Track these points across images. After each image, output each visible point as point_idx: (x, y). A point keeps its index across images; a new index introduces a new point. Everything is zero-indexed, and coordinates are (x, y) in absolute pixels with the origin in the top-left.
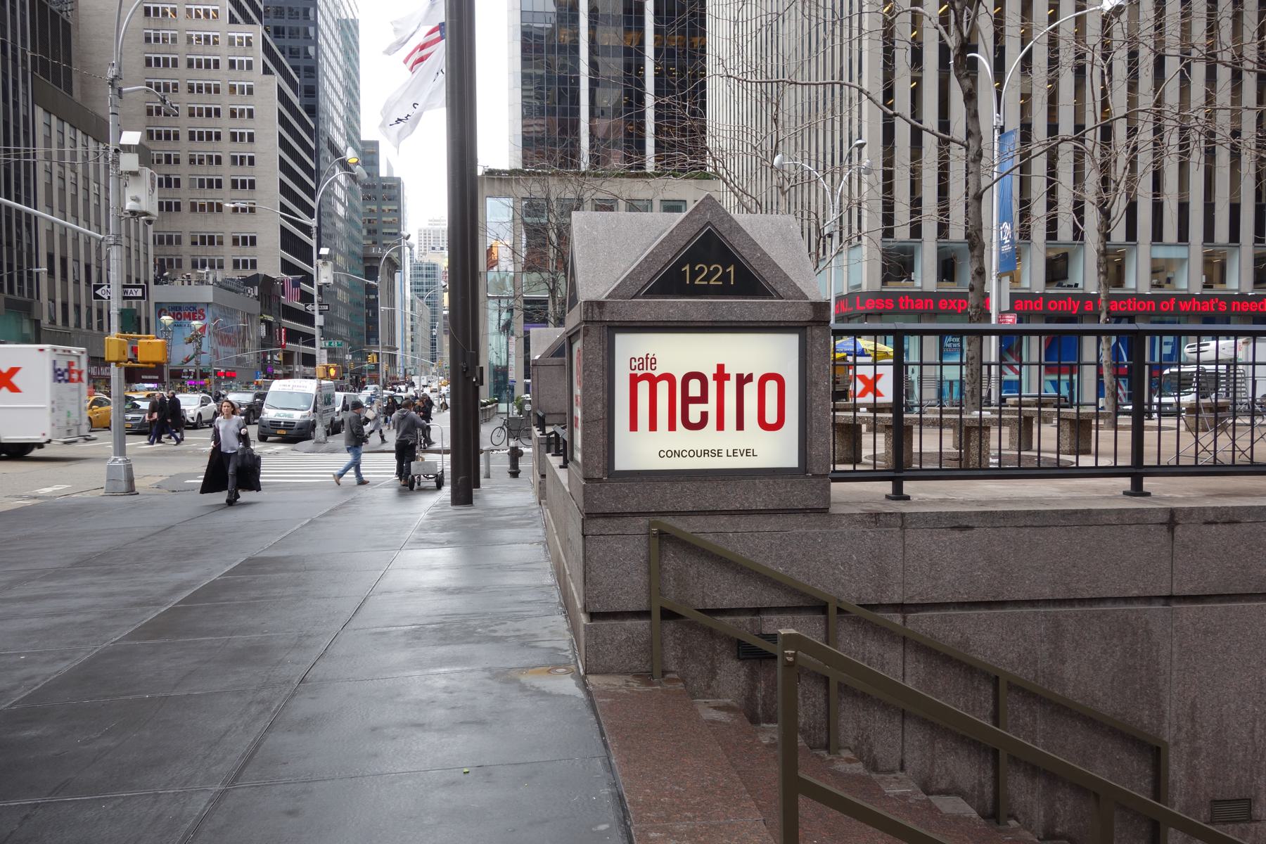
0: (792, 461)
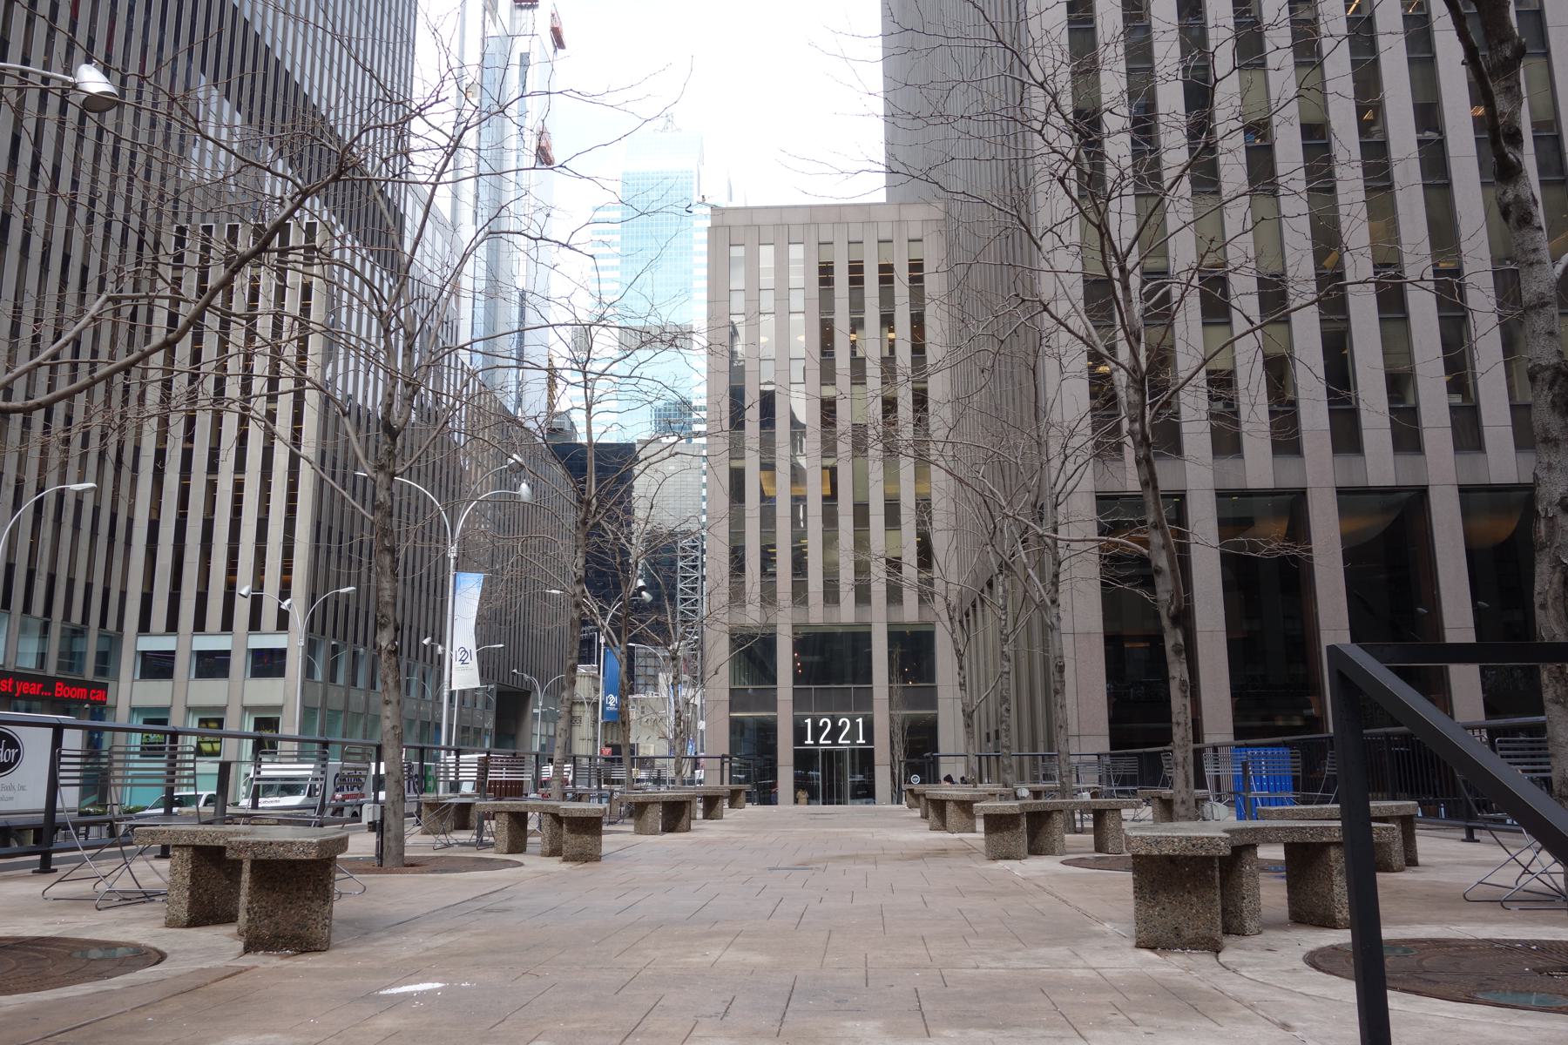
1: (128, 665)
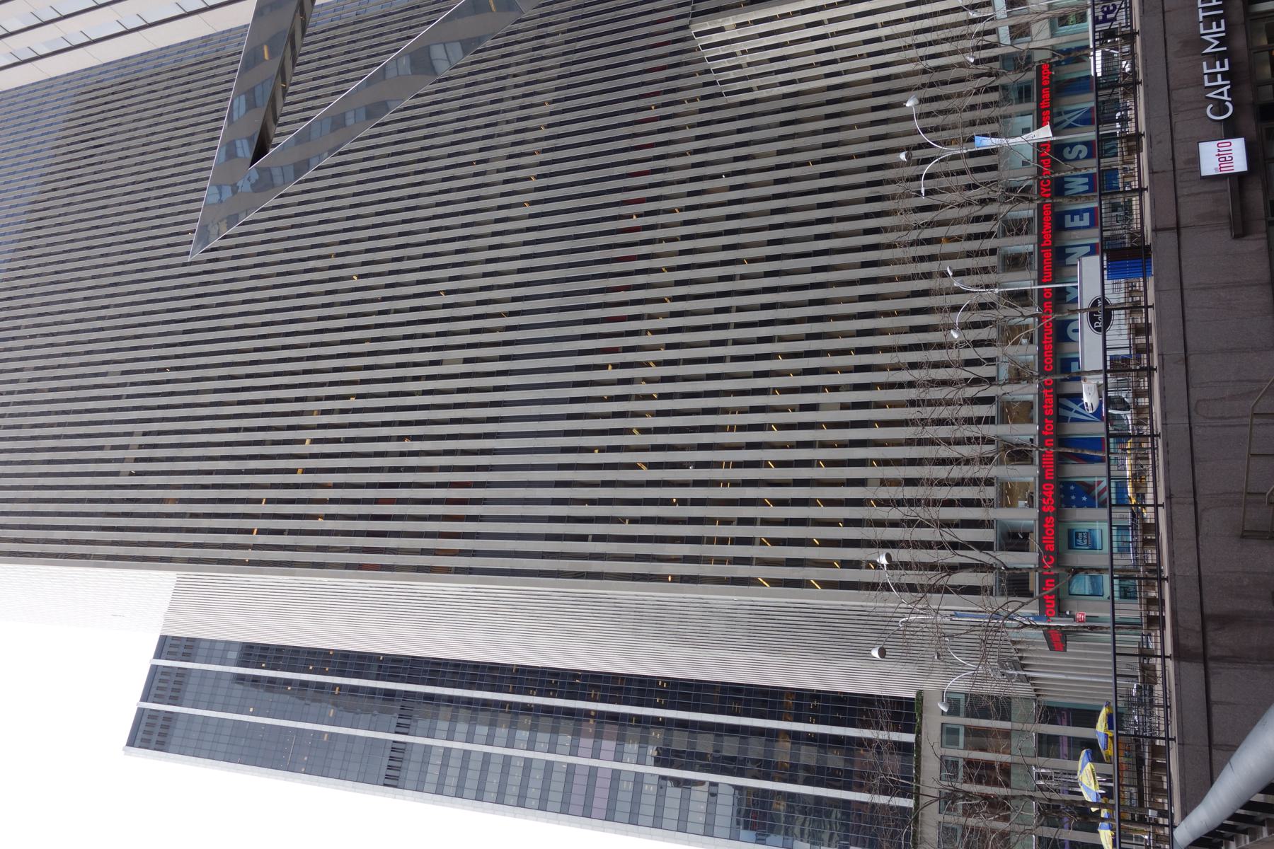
0: (1201, 145)
1: (1022, 45)
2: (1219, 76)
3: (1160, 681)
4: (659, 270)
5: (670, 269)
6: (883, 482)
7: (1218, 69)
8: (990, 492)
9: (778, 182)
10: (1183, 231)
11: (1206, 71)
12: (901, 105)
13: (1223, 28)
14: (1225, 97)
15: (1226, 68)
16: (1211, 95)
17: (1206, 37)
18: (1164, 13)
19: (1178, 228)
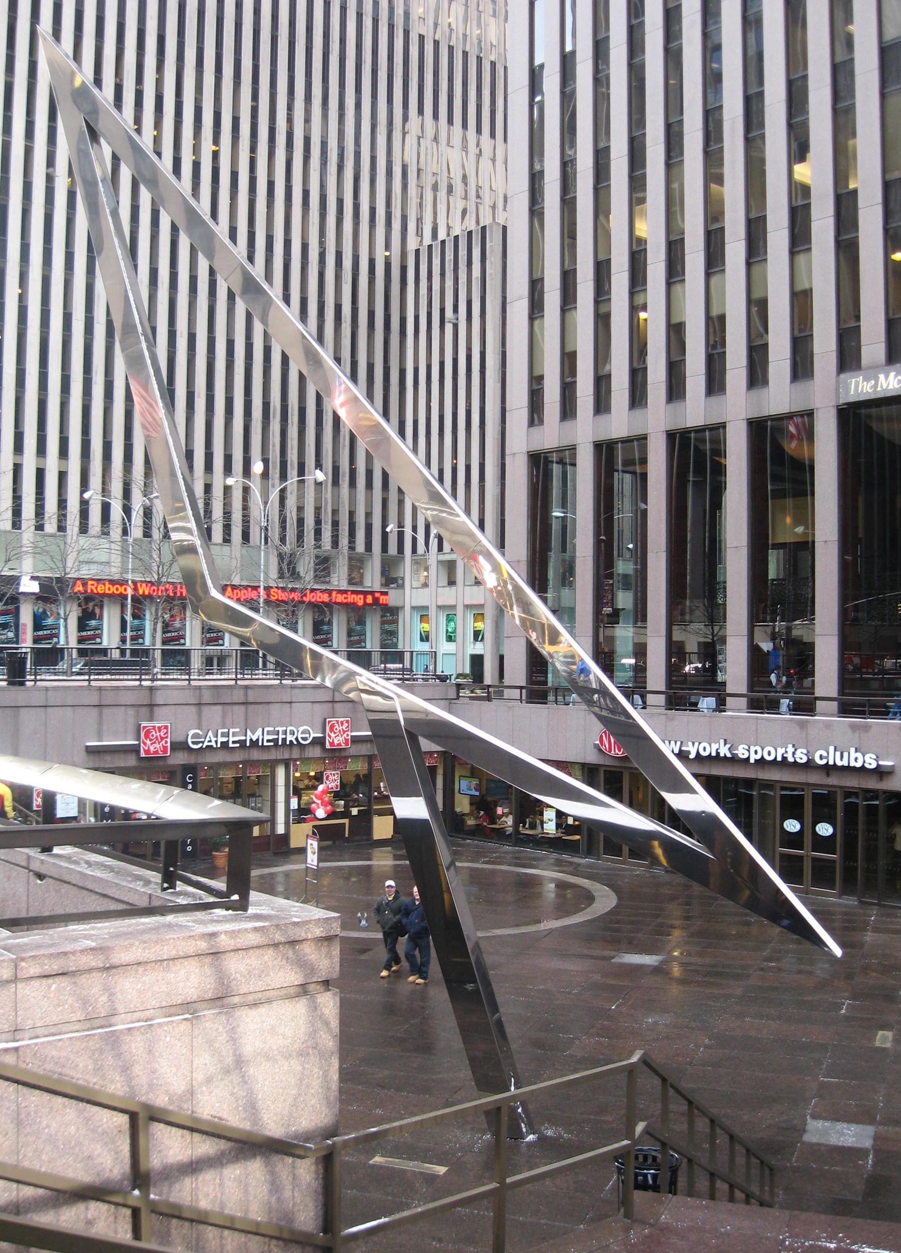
2: (225, 739)
3: (179, 677)
4: (216, 141)
5: (216, 155)
6: (40, 474)
7: (232, 739)
8: (360, 547)
9: (338, 308)
10: (330, 705)
11: (231, 731)
12: (319, 465)
13: (265, 744)
14: (206, 744)
15: (231, 745)
16: (210, 733)
17: (260, 730)
18: (291, 703)
19: (245, 703)
